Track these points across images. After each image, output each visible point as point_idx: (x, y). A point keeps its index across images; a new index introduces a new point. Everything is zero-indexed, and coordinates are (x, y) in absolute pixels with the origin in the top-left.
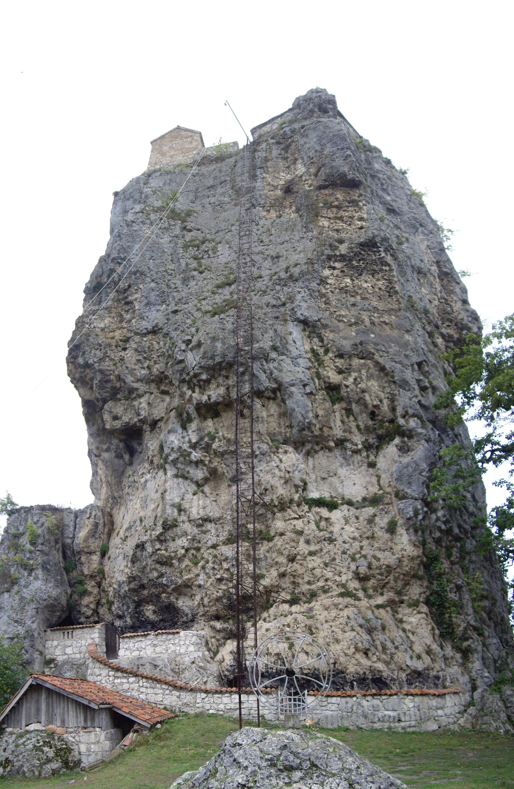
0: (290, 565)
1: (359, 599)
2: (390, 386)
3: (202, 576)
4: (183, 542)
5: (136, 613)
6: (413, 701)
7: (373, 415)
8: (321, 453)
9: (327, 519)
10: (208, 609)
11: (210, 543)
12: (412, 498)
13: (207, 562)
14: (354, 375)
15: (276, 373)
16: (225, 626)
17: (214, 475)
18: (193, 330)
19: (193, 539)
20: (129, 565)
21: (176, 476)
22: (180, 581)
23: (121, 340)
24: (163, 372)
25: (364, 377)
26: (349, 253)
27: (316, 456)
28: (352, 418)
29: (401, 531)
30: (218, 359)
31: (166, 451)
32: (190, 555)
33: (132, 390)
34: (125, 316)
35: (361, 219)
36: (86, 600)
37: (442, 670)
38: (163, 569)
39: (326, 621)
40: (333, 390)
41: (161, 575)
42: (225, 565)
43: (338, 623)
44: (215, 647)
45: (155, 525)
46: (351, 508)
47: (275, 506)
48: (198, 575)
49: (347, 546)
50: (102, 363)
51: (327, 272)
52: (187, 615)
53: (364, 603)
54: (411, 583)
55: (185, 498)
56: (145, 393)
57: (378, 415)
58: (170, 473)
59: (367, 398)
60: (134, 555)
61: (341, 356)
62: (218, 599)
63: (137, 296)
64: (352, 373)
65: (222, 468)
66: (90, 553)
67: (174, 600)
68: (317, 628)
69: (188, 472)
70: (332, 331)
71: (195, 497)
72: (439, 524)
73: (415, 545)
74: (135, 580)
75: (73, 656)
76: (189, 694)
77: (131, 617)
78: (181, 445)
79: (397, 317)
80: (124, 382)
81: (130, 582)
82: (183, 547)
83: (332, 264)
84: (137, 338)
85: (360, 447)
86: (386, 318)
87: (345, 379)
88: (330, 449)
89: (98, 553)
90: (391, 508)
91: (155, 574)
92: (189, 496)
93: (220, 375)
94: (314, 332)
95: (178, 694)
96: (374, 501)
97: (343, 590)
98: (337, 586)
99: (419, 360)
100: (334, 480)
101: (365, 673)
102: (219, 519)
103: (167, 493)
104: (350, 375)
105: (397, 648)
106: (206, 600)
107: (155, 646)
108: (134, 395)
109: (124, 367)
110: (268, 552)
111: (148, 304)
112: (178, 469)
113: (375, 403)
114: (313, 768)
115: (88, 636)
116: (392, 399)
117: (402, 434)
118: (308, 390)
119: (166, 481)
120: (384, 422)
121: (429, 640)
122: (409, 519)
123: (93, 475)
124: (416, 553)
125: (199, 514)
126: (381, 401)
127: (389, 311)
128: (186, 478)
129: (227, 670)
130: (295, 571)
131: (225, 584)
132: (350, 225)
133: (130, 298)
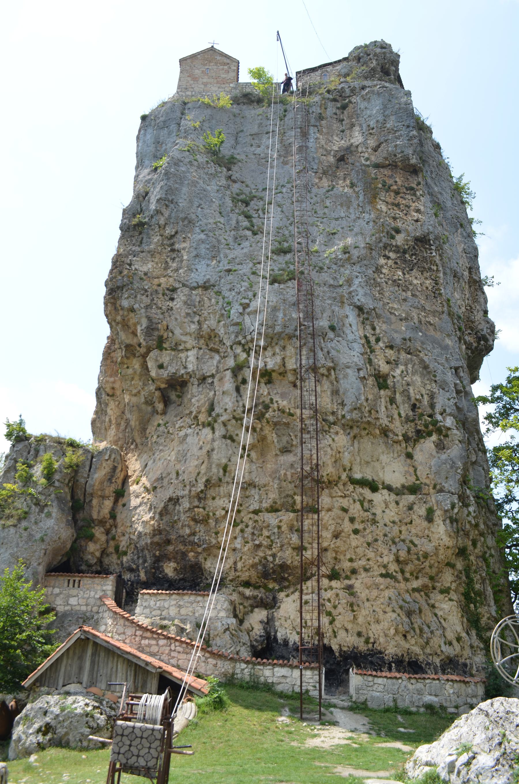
0: (334, 540)
2: (430, 384)
5: (154, 568)
6: (452, 687)
7: (414, 407)
9: (371, 501)
11: (252, 508)
12: (449, 492)
13: (247, 526)
14: (402, 367)
15: (333, 353)
16: (256, 593)
18: (250, 294)
20: (157, 517)
21: (224, 437)
25: (409, 371)
28: (394, 406)
29: (438, 520)
34: (170, 264)
35: (418, 211)
36: (92, 547)
37: (470, 658)
39: (368, 600)
41: (194, 534)
43: (379, 602)
44: (241, 614)
46: (392, 494)
47: (324, 482)
49: (387, 529)
51: (382, 261)
53: (403, 585)
54: (444, 571)
57: (419, 408)
58: (217, 433)
59: (411, 391)
60: (165, 508)
61: (391, 347)
63: (184, 245)
67: (203, 561)
68: (358, 606)
70: (384, 322)
72: (470, 518)
73: (450, 536)
74: (160, 534)
75: (78, 608)
76: (228, 663)
77: (146, 572)
79: (440, 319)
81: (154, 535)
84: (186, 290)
86: (431, 319)
87: (392, 369)
89: (112, 499)
90: (429, 499)
91: (187, 531)
95: (214, 662)
96: (414, 489)
97: (384, 572)
98: (379, 566)
99: (457, 365)
100: (376, 464)
101: (403, 655)
103: (215, 452)
104: (397, 367)
105: (432, 632)
106: (239, 565)
107: (180, 607)
113: (418, 397)
115: (99, 588)
116: (432, 396)
117: (439, 431)
118: (362, 374)
121: (459, 628)
122: (446, 511)
123: (96, 413)
124: (450, 544)
126: (422, 396)
127: (434, 313)
129: (256, 640)
130: (338, 547)
132: (406, 215)
133: (177, 246)
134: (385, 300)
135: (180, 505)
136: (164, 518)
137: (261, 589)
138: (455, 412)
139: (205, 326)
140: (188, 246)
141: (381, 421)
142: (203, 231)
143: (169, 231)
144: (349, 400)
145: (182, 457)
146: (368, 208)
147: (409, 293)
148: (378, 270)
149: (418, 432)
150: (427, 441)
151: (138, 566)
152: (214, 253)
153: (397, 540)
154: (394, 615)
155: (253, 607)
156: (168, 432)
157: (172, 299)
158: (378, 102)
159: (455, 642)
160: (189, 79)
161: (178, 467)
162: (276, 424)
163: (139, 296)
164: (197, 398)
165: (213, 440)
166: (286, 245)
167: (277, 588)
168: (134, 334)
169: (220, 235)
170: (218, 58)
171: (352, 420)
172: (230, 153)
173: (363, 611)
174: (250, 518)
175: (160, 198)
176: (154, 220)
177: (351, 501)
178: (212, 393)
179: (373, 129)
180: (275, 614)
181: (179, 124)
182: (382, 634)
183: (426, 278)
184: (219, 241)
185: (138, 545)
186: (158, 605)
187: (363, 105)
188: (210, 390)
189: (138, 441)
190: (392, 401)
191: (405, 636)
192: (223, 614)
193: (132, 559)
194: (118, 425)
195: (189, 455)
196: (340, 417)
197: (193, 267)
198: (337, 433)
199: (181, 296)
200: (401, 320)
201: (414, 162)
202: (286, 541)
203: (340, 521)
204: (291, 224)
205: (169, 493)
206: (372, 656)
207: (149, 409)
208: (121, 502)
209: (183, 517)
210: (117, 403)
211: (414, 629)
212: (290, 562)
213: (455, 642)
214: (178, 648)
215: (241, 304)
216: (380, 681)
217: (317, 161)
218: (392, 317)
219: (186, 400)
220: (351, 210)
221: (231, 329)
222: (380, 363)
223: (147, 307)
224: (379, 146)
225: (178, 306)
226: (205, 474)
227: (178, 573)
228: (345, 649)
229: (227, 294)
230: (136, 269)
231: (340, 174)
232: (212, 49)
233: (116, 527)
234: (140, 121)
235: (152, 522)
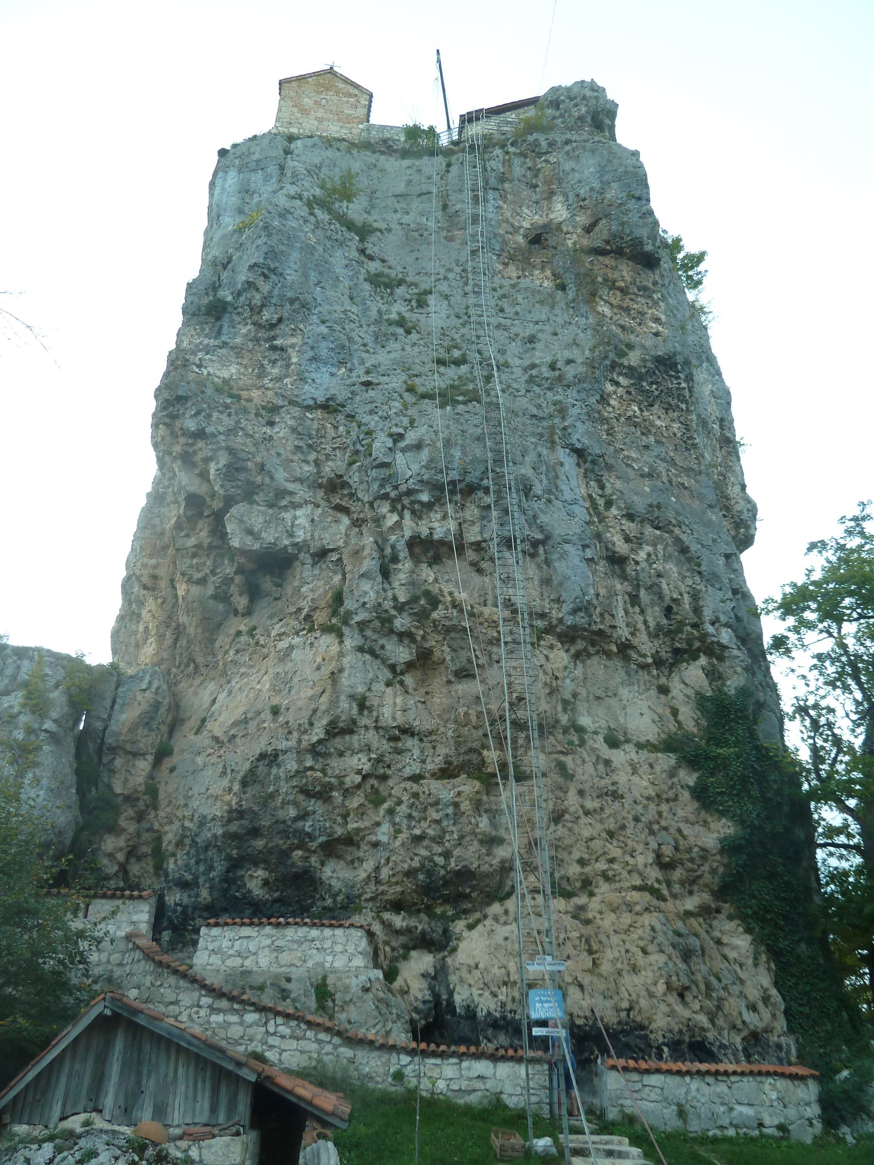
1: (664, 900)
3: (386, 828)
4: (361, 762)
6: (774, 1087)
7: (668, 611)
8: (595, 659)
10: (385, 888)
11: (408, 772)
13: (400, 803)
16: (413, 922)
17: (424, 661)
18: (406, 421)
19: (379, 760)
20: (236, 787)
21: (361, 649)
22: (339, 831)
23: (264, 408)
24: (341, 476)
26: (640, 367)
27: (588, 662)
30: (454, 475)
31: (349, 604)
32: (368, 786)
33: (282, 493)
34: (269, 368)
35: (657, 320)
36: (110, 843)
38: (313, 805)
40: (616, 561)
41: (304, 816)
42: (434, 815)
43: (635, 936)
45: (311, 724)
48: (378, 824)
49: (639, 808)
50: (232, 437)
51: (609, 388)
55: (373, 689)
56: (306, 502)
57: (677, 614)
58: (348, 643)
59: (664, 586)
60: (252, 771)
61: (630, 517)
62: (410, 873)
63: (294, 340)
64: (644, 546)
65: (443, 651)
66: (135, 755)
67: (318, 865)
70: (618, 478)
71: (389, 690)
76: (375, 1054)
78: (381, 601)
80: (272, 478)
81: (230, 821)
82: (359, 772)
83: (615, 376)
84: (296, 411)
85: (650, 660)
86: (684, 480)
88: (608, 655)
89: (150, 758)
91: (292, 812)
92: (379, 687)
94: (593, 471)
97: (638, 882)
98: (629, 872)
100: (613, 701)
102: (431, 733)
103: (345, 674)
104: (641, 548)
106: (385, 873)
107: (279, 949)
108: (284, 503)
109: (273, 452)
111: (314, 359)
113: (675, 596)
114: (621, 1155)
116: (695, 596)
117: (710, 653)
118: (589, 553)
119: (341, 654)
120: (686, 625)
125: (394, 719)
126: (681, 594)
129: (416, 1010)
130: (559, 839)
131: (427, 848)
132: (640, 324)
133: (278, 342)
134: (617, 445)
136: (249, 789)
137: (422, 915)
138: (733, 621)
139: (328, 469)
140: (300, 343)
141: (620, 632)
142: (324, 322)
144: (569, 596)
145: (283, 684)
146: (584, 308)
147: (652, 439)
148: (604, 399)
149: (676, 652)
150: (690, 667)
151: (197, 878)
152: (341, 356)
153: (656, 827)
154: (662, 959)
155: (408, 948)
156: (257, 643)
157: (271, 424)
158: (591, 162)
159: (760, 1006)
160: (295, 110)
161: (275, 701)
162: (448, 630)
163: (215, 415)
164: (310, 586)
165: (341, 654)
166: (456, 354)
167: (450, 913)
168: (204, 475)
169: (353, 330)
170: (341, 85)
171: (574, 627)
172: (362, 219)
173: (608, 952)
174: (405, 789)
175: (255, 265)
176: (242, 299)
177: (579, 761)
178: (337, 578)
179: (584, 200)
180: (449, 960)
181: (282, 168)
182: (644, 993)
183: (673, 421)
184: (350, 339)
185: (198, 840)
186: (236, 948)
187: (568, 166)
188: (335, 573)
189: (200, 660)
190: (634, 599)
191: (681, 996)
192: (359, 962)
193: (186, 865)
194: (161, 637)
195: (296, 679)
196: (555, 622)
197: (307, 374)
198: (551, 647)
199: (287, 419)
200: (642, 476)
201: (636, 257)
202: (468, 829)
203: (561, 794)
204: (463, 325)
205: (261, 745)
206: (626, 1033)
207: (221, 607)
208: (168, 763)
209: (284, 788)
210: (160, 601)
211: (695, 982)
212: (475, 865)
213: (760, 1006)
214: (280, 1028)
215: (391, 435)
216: (655, 1080)
217: (500, 240)
218: (629, 470)
219: (289, 590)
220: (557, 311)
221: (374, 473)
222: (615, 539)
223: (231, 432)
224: (594, 225)
225: (281, 435)
227: (270, 889)
228: (579, 1022)
229: (366, 419)
230: (209, 374)
231: (536, 260)
232: (331, 71)
233: (156, 808)
234: (216, 158)
235: (227, 798)
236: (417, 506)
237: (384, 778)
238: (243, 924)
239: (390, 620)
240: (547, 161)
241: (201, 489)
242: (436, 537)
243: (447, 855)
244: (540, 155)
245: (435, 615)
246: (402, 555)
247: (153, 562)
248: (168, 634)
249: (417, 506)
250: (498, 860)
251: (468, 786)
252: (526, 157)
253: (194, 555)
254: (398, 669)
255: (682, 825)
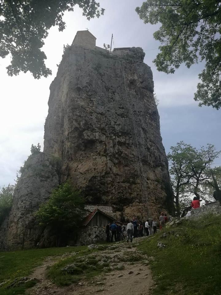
4: (110, 179)
13: (116, 186)
17: (120, 163)
19: (113, 179)
20: (88, 182)
21: (110, 160)
30: (125, 131)
31: (108, 152)
33: (94, 129)
41: (100, 188)
48: (113, 190)
51: (147, 117)
52: (104, 202)
56: (98, 132)
58: (108, 159)
61: (150, 141)
63: (94, 99)
69: (113, 160)
71: (114, 167)
80: (93, 127)
81: (87, 188)
89: (67, 176)
91: (98, 187)
92: (113, 166)
93: (124, 135)
97: (153, 202)
102: (121, 175)
103: (108, 164)
110: (135, 187)
112: (111, 158)
116: (160, 156)
119: (107, 160)
128: (112, 161)
133: (92, 99)
135: (96, 179)
143: (89, 93)
154: (156, 213)
156: (88, 156)
164: (99, 147)
165: (107, 160)
168: (79, 124)
175: (88, 83)
187: (138, 67)
188: (104, 145)
190: (150, 156)
195: (98, 164)
205: (93, 175)
223: (85, 117)
226: (105, 170)
229: (109, 118)
236: (118, 136)
237: (114, 182)
238: (92, 205)
239: (115, 155)
240: (133, 65)
241: (78, 126)
242: (122, 141)
243: (123, 195)
244: (132, 64)
245: (122, 155)
246: (116, 144)
247: (57, 137)
248: (60, 152)
249: (118, 136)
250: (131, 197)
251: (128, 185)
252: (129, 63)
253: (73, 138)
254: (116, 164)
255: (158, 194)
